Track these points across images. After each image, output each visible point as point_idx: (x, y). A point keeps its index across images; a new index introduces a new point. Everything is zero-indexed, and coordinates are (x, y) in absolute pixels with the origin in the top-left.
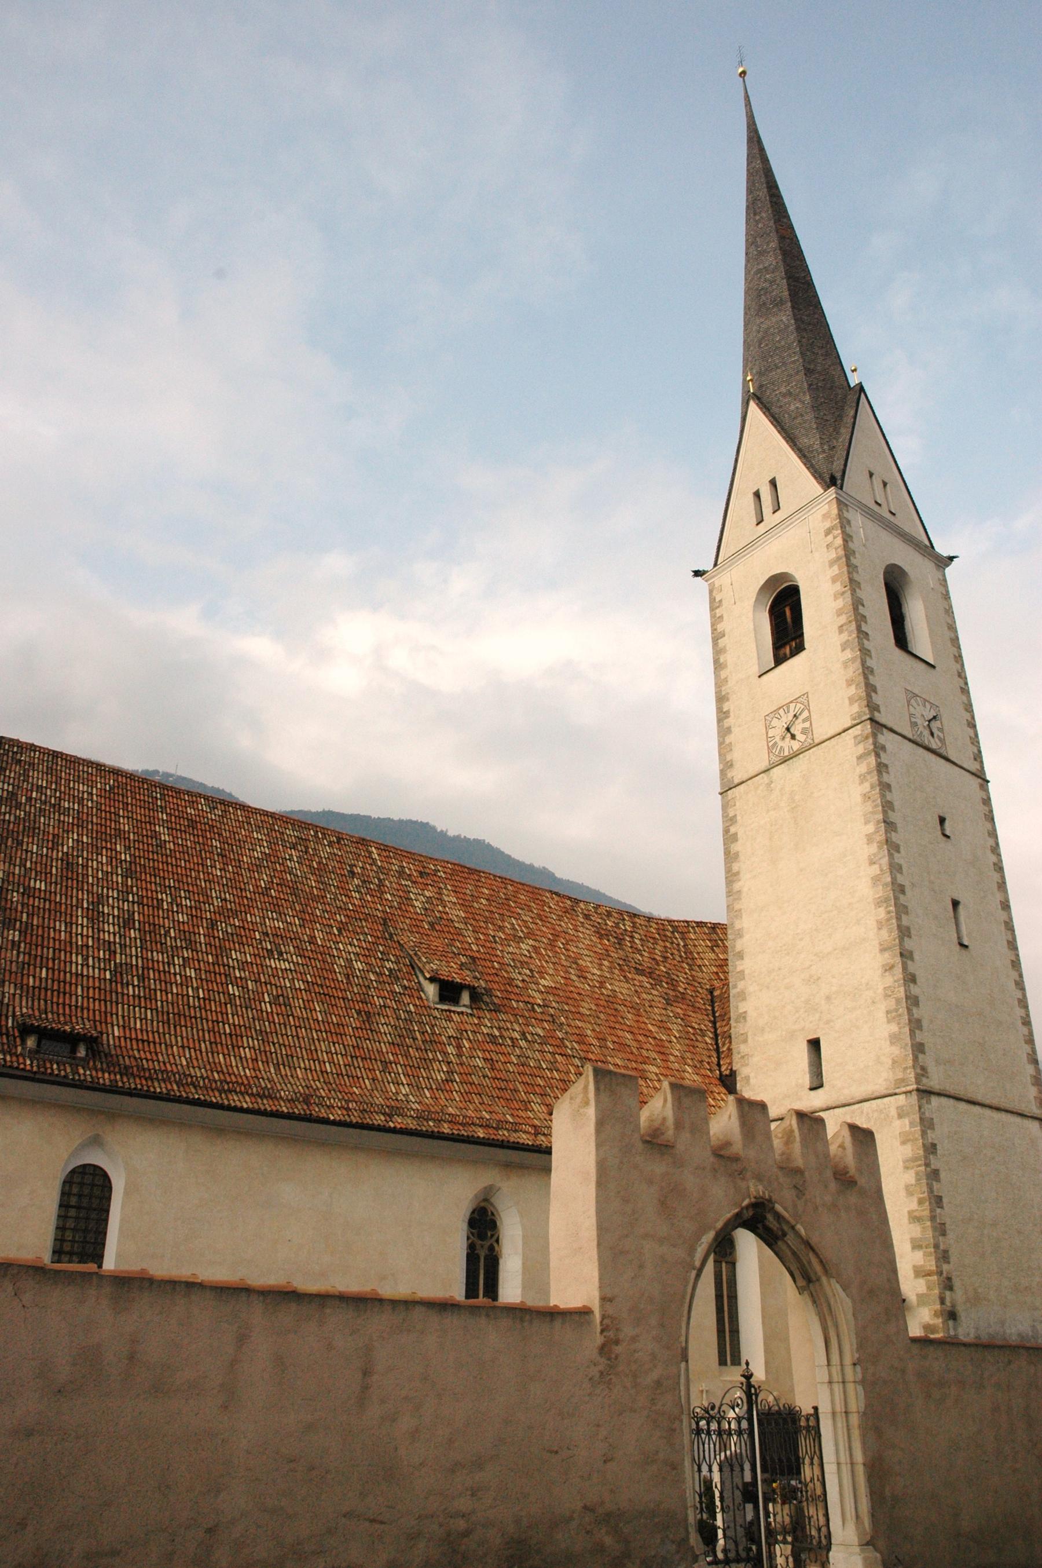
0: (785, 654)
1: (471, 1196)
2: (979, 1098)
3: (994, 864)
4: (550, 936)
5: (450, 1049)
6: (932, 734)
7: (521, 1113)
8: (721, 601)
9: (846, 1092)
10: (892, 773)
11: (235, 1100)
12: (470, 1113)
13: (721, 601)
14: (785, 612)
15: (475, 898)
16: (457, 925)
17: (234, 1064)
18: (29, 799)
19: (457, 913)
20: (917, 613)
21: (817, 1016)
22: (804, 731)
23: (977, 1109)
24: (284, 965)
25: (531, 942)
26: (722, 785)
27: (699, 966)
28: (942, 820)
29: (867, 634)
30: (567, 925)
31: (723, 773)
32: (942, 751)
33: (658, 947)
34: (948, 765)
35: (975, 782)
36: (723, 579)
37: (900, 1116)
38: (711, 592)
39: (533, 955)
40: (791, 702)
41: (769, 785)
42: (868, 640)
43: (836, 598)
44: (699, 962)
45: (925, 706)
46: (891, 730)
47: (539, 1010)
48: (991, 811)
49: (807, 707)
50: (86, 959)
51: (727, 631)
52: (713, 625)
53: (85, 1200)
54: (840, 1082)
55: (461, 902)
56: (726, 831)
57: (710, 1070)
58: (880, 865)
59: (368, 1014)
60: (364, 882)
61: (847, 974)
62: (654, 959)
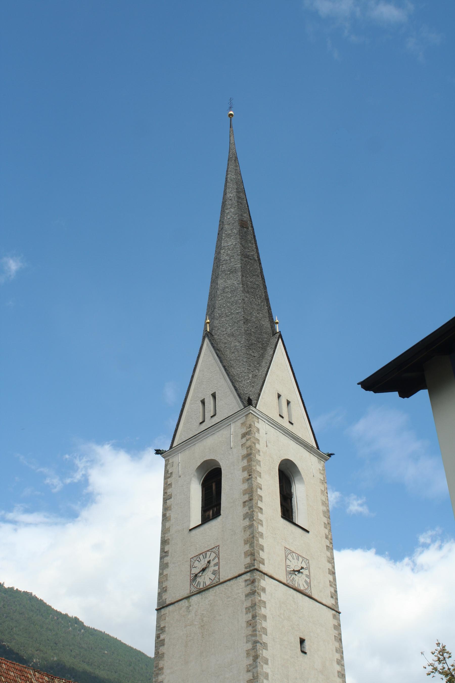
0: (209, 515)
3: (338, 672)
8: (171, 473)
13: (171, 473)
14: (212, 485)
26: (159, 604)
28: (302, 641)
32: (308, 592)
38: (166, 466)
40: (208, 551)
41: (188, 608)
42: (262, 513)
45: (298, 560)
48: (340, 634)
49: (218, 556)
52: (165, 489)
56: (158, 637)
58: (253, 673)
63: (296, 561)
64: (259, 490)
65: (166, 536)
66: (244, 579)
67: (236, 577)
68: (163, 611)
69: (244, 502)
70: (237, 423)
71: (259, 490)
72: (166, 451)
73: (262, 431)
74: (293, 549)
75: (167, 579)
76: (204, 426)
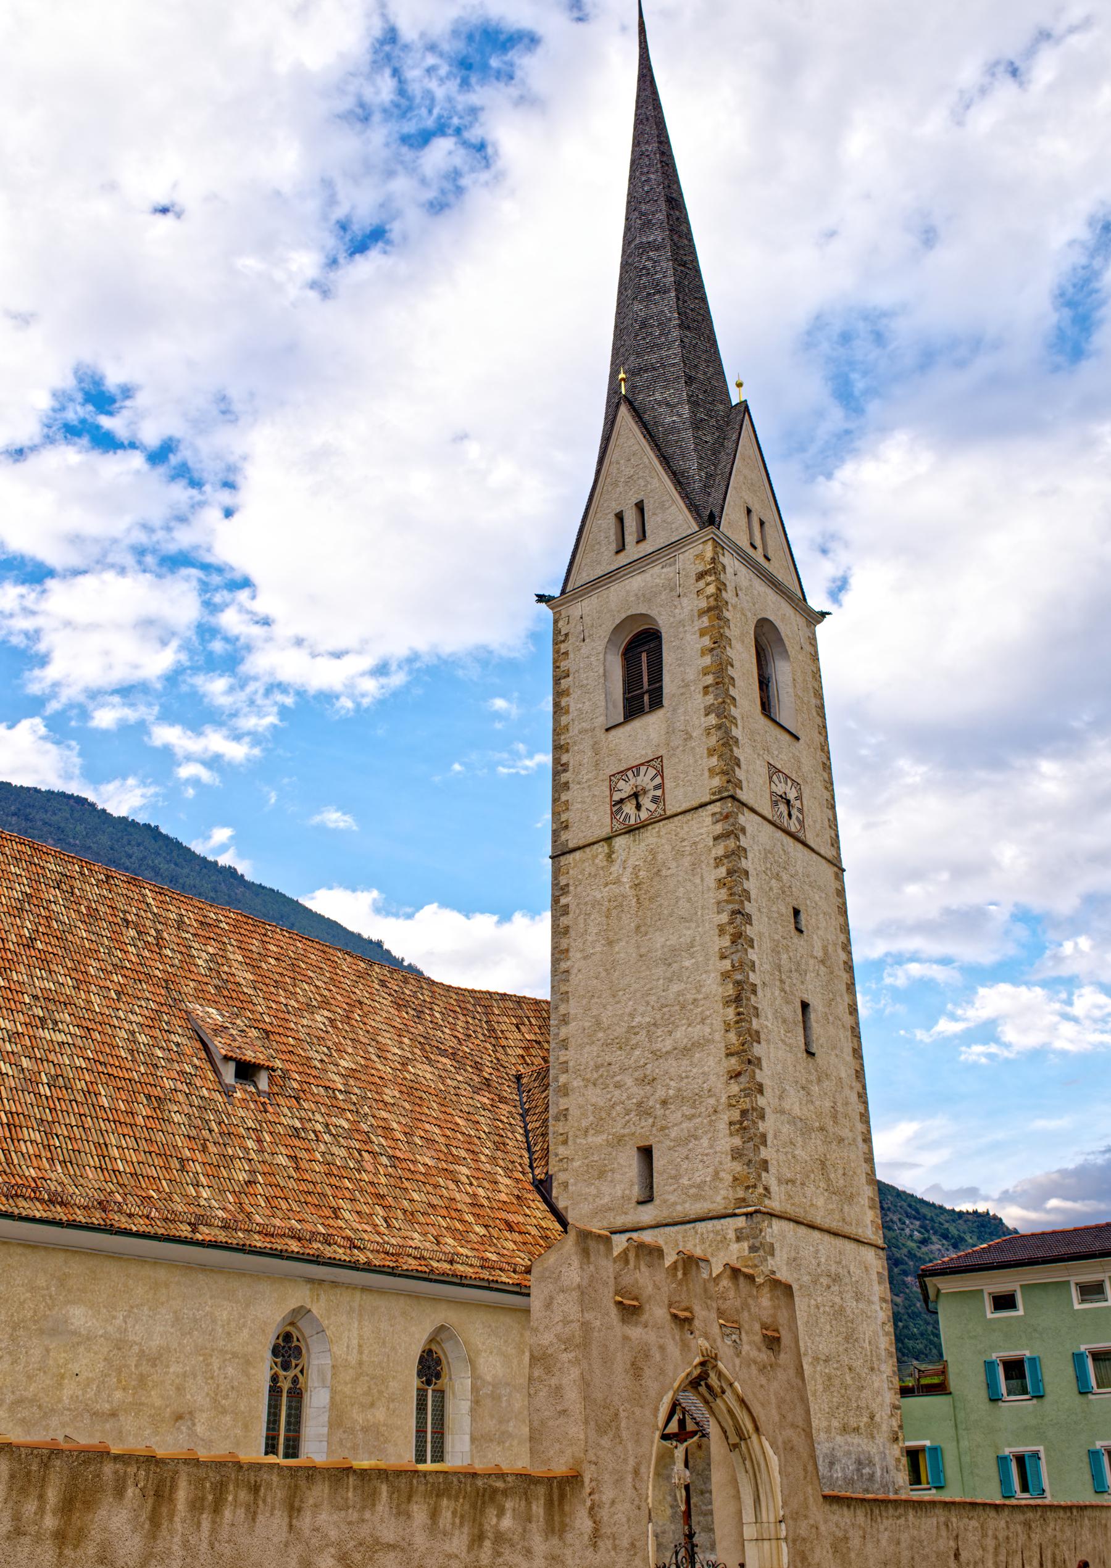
2: (818, 1221)
4: (345, 1006)
5: (250, 1144)
6: (790, 815)
7: (331, 1222)
8: (567, 635)
9: (679, 1208)
10: (750, 858)
11: (26, 1207)
12: (277, 1222)
13: (567, 635)
15: (263, 957)
16: (246, 990)
17: (16, 1162)
19: (244, 976)
20: (783, 672)
21: (651, 1120)
22: (655, 800)
23: (816, 1234)
25: (326, 1013)
27: (503, 1047)
28: (796, 912)
29: (734, 699)
30: (360, 993)
31: (556, 834)
33: (459, 1022)
34: (806, 851)
35: (830, 871)
36: (576, 610)
37: (738, 1239)
39: (330, 1029)
40: (642, 764)
43: (703, 654)
44: (504, 1042)
47: (341, 1097)
48: (845, 904)
51: (572, 671)
52: (555, 661)
54: (672, 1199)
55: (248, 961)
57: (523, 1173)
60: (139, 933)
61: (687, 1077)
62: (455, 1037)
63: (783, 785)
64: (729, 668)
65: (563, 737)
66: (710, 812)
67: (696, 808)
68: (563, 860)
69: (707, 687)
70: (687, 554)
71: (729, 668)
72: (554, 598)
73: (729, 570)
74: (779, 767)
75: (567, 809)
76: (623, 559)
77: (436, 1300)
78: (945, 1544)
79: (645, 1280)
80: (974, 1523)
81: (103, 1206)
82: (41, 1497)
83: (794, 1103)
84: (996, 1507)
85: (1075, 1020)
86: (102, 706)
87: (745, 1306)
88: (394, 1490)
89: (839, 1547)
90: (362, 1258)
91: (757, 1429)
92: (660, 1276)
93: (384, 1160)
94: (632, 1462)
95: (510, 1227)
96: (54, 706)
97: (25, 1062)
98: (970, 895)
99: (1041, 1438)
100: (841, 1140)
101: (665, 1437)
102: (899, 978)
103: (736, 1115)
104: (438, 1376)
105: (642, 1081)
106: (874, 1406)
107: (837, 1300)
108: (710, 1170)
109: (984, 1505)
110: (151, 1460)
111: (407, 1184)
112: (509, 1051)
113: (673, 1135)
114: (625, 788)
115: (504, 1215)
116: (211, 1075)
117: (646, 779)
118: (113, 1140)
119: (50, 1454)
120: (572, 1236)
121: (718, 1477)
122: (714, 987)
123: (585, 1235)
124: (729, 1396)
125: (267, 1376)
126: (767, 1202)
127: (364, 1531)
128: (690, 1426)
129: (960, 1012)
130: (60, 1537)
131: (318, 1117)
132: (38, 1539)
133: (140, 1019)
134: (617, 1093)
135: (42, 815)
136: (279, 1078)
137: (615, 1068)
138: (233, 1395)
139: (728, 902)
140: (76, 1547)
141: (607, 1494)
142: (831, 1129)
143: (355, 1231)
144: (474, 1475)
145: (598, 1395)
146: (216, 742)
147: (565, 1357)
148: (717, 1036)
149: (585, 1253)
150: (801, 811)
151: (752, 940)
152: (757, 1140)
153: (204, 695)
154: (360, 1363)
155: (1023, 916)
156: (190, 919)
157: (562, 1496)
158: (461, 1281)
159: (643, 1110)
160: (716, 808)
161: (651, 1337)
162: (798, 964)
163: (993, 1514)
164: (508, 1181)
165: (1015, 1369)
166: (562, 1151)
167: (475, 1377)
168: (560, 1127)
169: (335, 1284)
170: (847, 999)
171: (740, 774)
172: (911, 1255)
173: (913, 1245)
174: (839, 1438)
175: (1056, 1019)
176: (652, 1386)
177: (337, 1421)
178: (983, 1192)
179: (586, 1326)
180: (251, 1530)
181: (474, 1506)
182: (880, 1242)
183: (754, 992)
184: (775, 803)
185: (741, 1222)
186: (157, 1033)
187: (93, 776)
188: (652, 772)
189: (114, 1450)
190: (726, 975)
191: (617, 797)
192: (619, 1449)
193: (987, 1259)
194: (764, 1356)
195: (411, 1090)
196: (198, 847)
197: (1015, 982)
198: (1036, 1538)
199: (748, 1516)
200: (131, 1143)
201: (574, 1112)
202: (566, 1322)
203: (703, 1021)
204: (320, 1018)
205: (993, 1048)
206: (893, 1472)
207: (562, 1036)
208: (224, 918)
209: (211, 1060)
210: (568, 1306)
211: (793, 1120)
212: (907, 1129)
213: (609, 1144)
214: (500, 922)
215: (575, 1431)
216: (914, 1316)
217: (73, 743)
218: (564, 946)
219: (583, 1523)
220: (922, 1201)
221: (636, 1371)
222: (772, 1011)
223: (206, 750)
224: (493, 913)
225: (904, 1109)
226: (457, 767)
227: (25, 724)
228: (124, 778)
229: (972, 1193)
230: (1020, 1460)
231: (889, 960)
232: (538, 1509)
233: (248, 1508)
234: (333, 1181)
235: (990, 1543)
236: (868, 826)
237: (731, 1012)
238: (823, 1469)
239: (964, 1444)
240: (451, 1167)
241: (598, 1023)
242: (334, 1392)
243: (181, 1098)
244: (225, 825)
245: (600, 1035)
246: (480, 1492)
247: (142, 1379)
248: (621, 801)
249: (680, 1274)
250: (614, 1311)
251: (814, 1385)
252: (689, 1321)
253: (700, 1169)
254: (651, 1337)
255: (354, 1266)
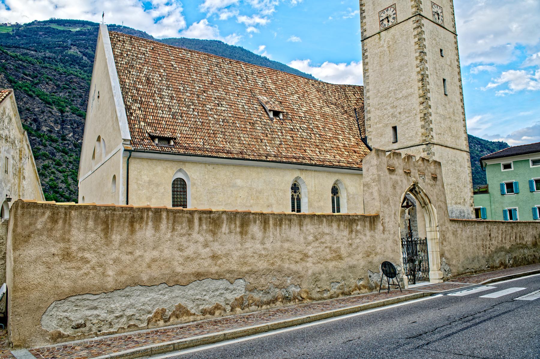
1: (292, 180)
2: (448, 145)
5: (279, 134)
6: (439, 19)
9: (405, 144)
11: (221, 155)
12: (289, 154)
15: (277, 80)
18: (127, 55)
19: (272, 87)
22: (394, 18)
23: (448, 149)
24: (223, 109)
28: (441, 50)
30: (306, 88)
32: (442, 25)
37: (424, 151)
44: (350, 99)
46: (426, 18)
50: (163, 111)
53: (179, 188)
56: (364, 54)
59: (252, 123)
77: (335, 173)
78: (486, 232)
79: (396, 162)
80: (496, 227)
81: (241, 153)
82: (235, 224)
83: (441, 110)
84: (503, 222)
85: (536, 80)
86: (223, 12)
87: (426, 168)
88: (327, 220)
89: (454, 233)
90: (314, 163)
91: (430, 202)
92: (401, 161)
93: (317, 135)
94: (393, 211)
95: (355, 152)
96: (209, 15)
97: (215, 116)
98: (501, 41)
99: (517, 204)
100: (456, 121)
101: (402, 207)
102: (475, 71)
103: (422, 115)
104: (337, 193)
105: (393, 107)
106: (465, 197)
107: (454, 167)
108: (415, 132)
109: (499, 222)
110: (262, 214)
111: (325, 142)
112: (352, 103)
113: (403, 123)
114: (384, 16)
115: (353, 149)
116: (266, 116)
117: (390, 12)
118: (242, 135)
119: (236, 213)
120: (373, 151)
121: (419, 215)
122: (416, 77)
123: (377, 151)
124: (422, 193)
125: (291, 194)
126: (432, 140)
127: (320, 230)
128: (410, 204)
129: (496, 80)
130: (241, 233)
131: (298, 125)
132: (236, 233)
133: (245, 102)
134: (385, 111)
135: (209, 47)
136: (286, 115)
137: (384, 104)
138: (282, 200)
139: (418, 49)
140: (245, 235)
141: (387, 220)
142: (453, 118)
143: (311, 155)
144: (349, 216)
145: (383, 194)
146: (257, 20)
147: (373, 184)
148: (416, 92)
149: (378, 155)
150: (442, 17)
151: (427, 61)
152: (429, 122)
153: (252, 5)
154: (315, 191)
155: (519, 47)
156: (255, 71)
157: (374, 220)
158: (342, 167)
159: (393, 116)
160: (414, 19)
161: (398, 178)
162: (442, 67)
163: (501, 224)
164: (354, 139)
165: (510, 186)
166: (369, 129)
167: (348, 193)
168: (368, 123)
169: (306, 170)
170: (458, 77)
171: (422, 6)
172: (477, 155)
173: (478, 152)
174: (454, 206)
175: (529, 80)
176: (399, 191)
177: (310, 205)
178: (501, 136)
179: (379, 176)
180: (290, 231)
181: (349, 223)
182: (468, 149)
183: (428, 77)
184: (434, 15)
185: (424, 146)
186: (250, 105)
187: (224, 35)
188: (392, 9)
189: (252, 212)
190: (418, 73)
191: (381, 19)
192: (390, 208)
193: (502, 154)
194: (432, 182)
195: (324, 115)
196: (255, 52)
197: (515, 69)
198: (515, 231)
199: (428, 225)
200: (247, 136)
201: (372, 118)
202: (373, 175)
203: (411, 87)
204: (296, 96)
205: (507, 91)
206: (471, 215)
207: (368, 96)
208: (265, 70)
209: (266, 111)
210: (374, 170)
211: (440, 116)
212: (477, 118)
213: (383, 126)
214: (347, 65)
215: (377, 203)
216: (478, 173)
217: (216, 25)
218: (367, 68)
219: (380, 227)
220: (481, 139)
221: (394, 187)
222: (433, 83)
223: (254, 22)
224: (345, 62)
225: (475, 113)
226: (330, 18)
227: (202, 21)
228: (232, 34)
229: (498, 136)
230: (510, 211)
231: (472, 66)
232: (367, 224)
233: (289, 225)
234: (304, 142)
235: (500, 232)
236: (465, 22)
237: (420, 84)
238: (450, 214)
239: (493, 207)
240: (337, 136)
241: (379, 91)
242: (309, 198)
243: (259, 122)
244: (262, 45)
245: (379, 94)
246: (350, 221)
247: (257, 197)
248: (383, 20)
249: (406, 160)
250: (387, 171)
251: (447, 191)
252: (409, 173)
253: (412, 132)
254: (398, 178)
255: (312, 165)
